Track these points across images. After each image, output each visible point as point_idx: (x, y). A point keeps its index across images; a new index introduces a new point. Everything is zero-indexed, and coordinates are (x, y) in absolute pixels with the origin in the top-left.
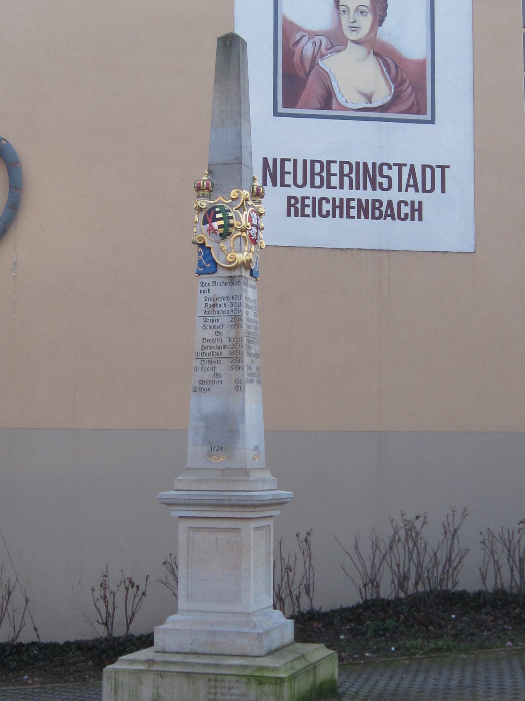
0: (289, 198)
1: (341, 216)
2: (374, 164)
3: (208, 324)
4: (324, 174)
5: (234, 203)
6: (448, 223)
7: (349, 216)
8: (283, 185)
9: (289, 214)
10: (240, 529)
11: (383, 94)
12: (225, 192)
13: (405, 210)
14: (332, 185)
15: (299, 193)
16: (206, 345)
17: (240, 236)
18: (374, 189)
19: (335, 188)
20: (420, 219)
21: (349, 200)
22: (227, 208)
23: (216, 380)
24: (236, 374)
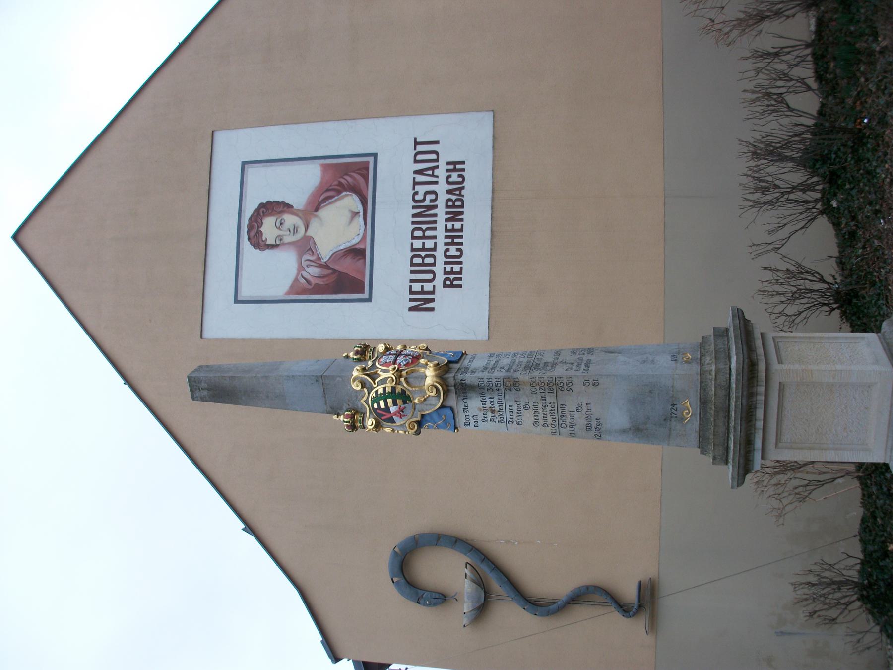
0: (445, 286)
1: (461, 237)
2: (414, 207)
3: (515, 419)
4: (423, 254)
5: (367, 385)
6: (465, 138)
7: (461, 230)
8: (433, 292)
9: (460, 286)
10: (780, 383)
11: (351, 201)
12: (357, 396)
13: (455, 177)
14: (432, 246)
15: (440, 277)
16: (541, 422)
17: (406, 379)
18: (436, 207)
19: (435, 243)
20: (463, 163)
21: (447, 230)
22: (373, 394)
23: (585, 410)
24: (578, 386)
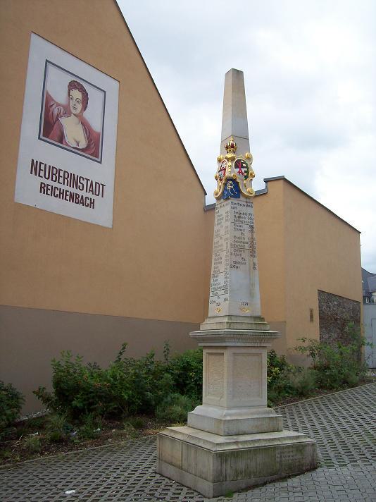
0: (42, 183)
6: (102, 213)
11: (83, 144)
